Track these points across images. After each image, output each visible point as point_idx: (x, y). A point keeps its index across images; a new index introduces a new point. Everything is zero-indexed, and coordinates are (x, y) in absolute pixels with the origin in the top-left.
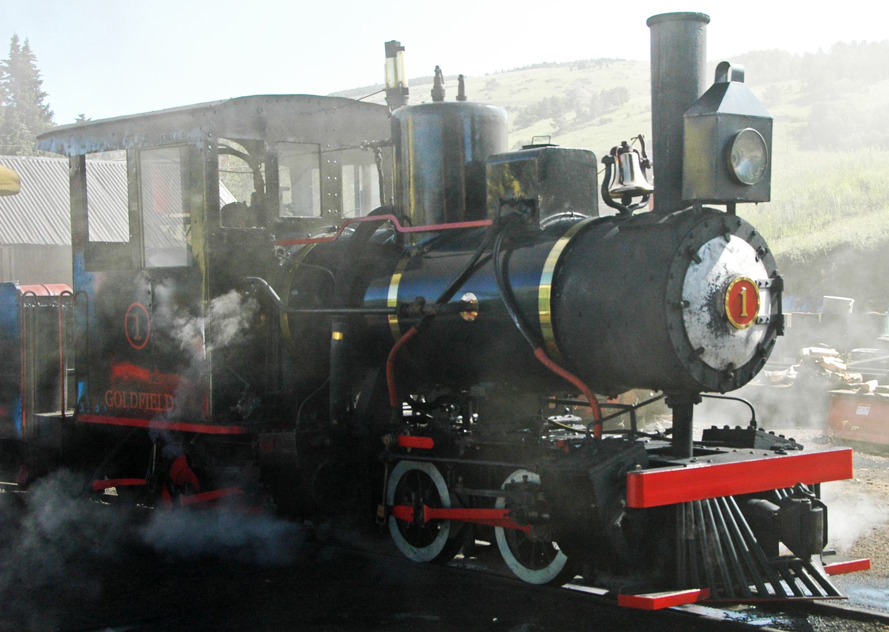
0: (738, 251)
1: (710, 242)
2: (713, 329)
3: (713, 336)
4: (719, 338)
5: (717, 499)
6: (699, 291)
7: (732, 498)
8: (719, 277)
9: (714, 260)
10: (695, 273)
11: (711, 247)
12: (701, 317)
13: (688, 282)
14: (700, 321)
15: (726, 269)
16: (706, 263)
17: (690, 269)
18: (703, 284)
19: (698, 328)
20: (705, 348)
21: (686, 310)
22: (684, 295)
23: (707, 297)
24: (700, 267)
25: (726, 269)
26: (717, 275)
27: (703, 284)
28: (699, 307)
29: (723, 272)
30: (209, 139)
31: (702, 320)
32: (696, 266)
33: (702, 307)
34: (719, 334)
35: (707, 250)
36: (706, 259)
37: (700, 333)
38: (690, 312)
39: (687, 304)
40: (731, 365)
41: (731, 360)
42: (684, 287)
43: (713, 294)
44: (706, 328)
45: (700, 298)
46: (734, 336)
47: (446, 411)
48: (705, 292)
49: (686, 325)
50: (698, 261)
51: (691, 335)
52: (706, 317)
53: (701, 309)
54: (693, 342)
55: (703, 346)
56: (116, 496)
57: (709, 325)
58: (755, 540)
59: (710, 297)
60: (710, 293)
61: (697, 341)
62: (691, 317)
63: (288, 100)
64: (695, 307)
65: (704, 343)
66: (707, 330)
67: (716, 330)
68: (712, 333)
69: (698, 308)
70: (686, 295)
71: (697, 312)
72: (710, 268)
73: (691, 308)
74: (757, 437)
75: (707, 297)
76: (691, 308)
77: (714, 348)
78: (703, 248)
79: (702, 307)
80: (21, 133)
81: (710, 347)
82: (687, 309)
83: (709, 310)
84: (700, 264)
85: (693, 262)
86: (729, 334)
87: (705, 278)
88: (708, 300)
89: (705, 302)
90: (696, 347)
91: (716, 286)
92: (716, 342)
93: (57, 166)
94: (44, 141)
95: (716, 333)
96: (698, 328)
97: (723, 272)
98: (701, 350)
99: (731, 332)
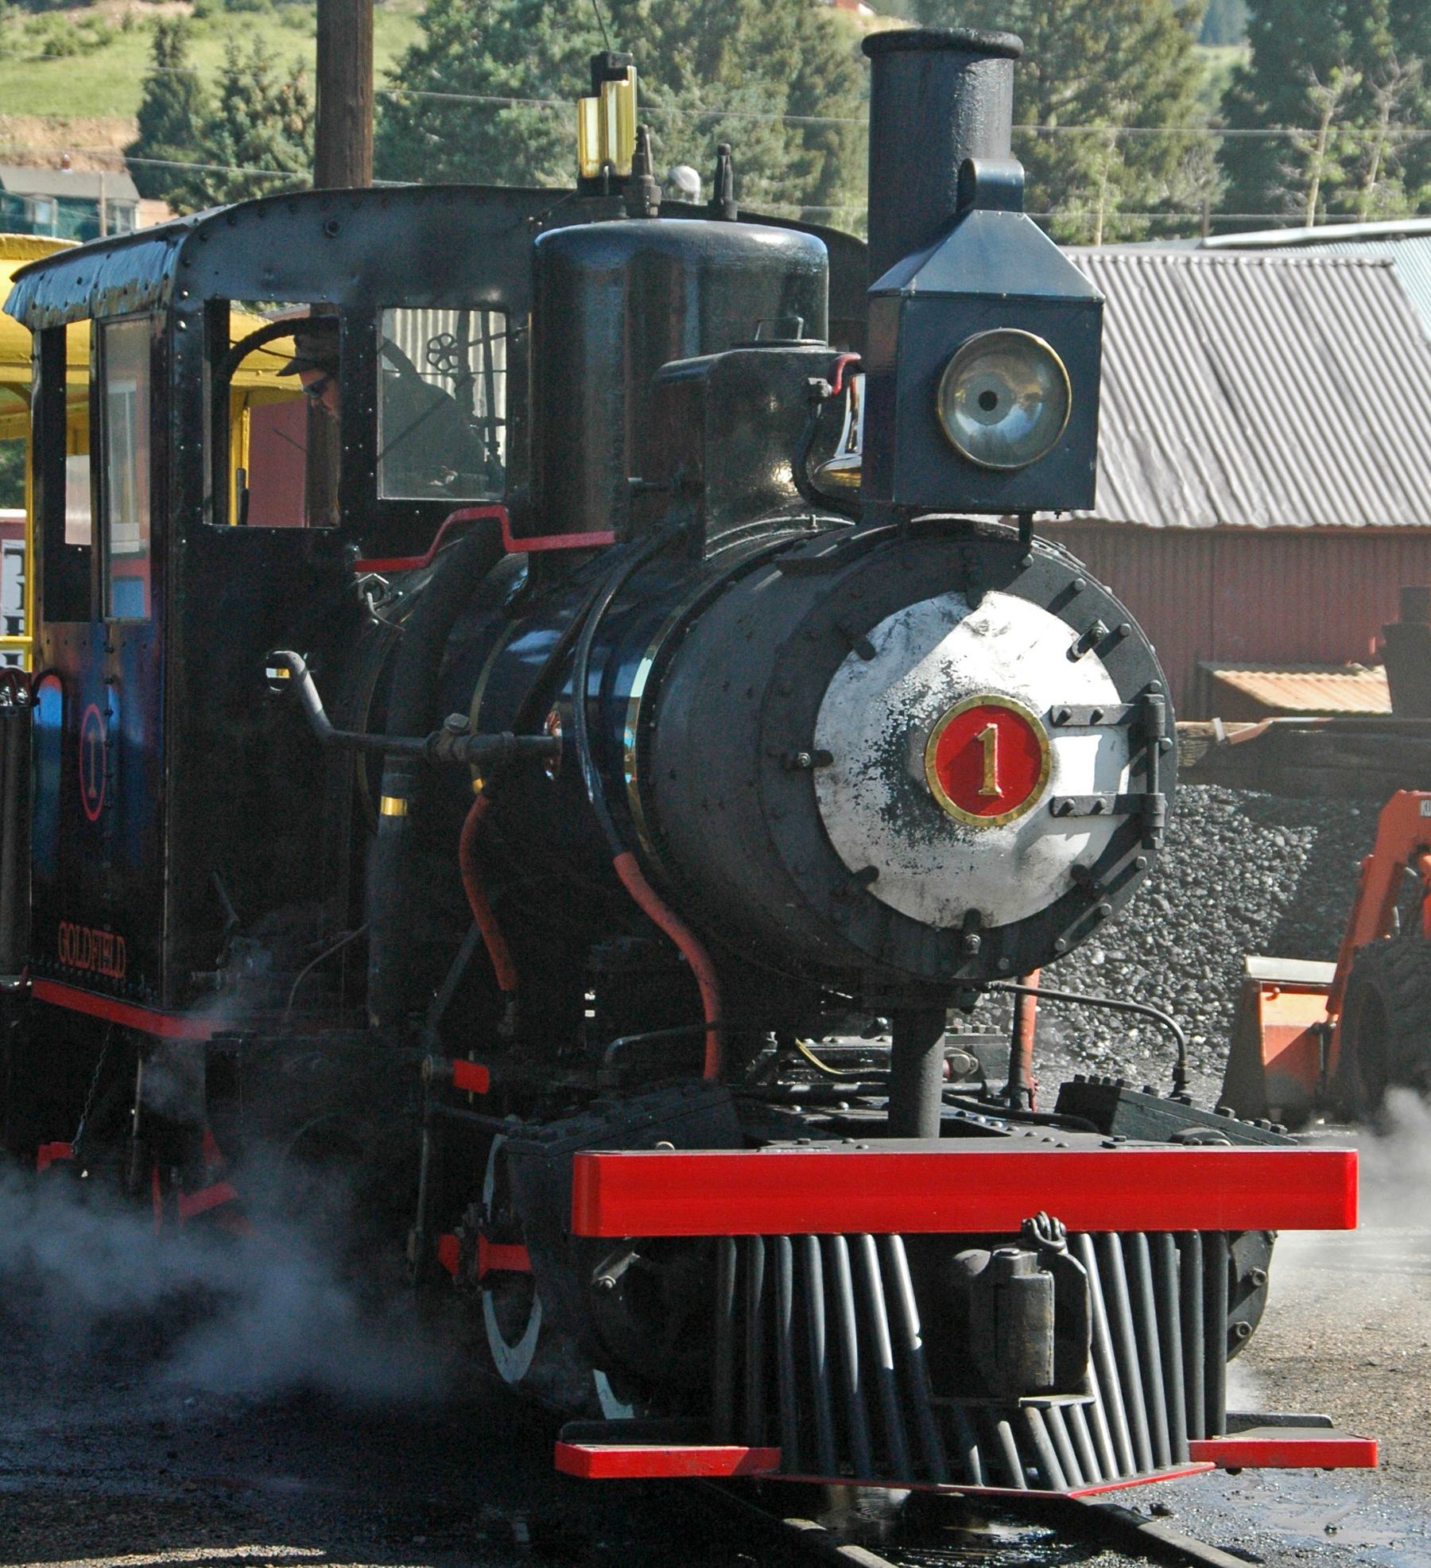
0: (1002, 632)
1: (913, 608)
2: (900, 823)
3: (902, 840)
4: (922, 847)
5: (821, 1237)
6: (861, 729)
7: (898, 1242)
8: (922, 695)
9: (917, 649)
10: (855, 684)
11: (911, 620)
12: (863, 792)
13: (833, 704)
14: (863, 802)
15: (948, 675)
16: (890, 661)
17: (841, 675)
18: (875, 709)
19: (856, 819)
20: (883, 869)
21: (821, 774)
22: (817, 736)
23: (881, 742)
24: (874, 671)
25: (948, 675)
26: (919, 687)
27: (875, 709)
28: (857, 767)
29: (937, 683)
30: (182, 305)
31: (867, 798)
32: (861, 667)
33: (866, 767)
34: (918, 835)
35: (899, 628)
36: (891, 650)
37: (864, 830)
38: (834, 779)
39: (824, 758)
40: (973, 918)
41: (973, 904)
42: (821, 717)
43: (899, 738)
44: (878, 818)
45: (864, 745)
46: (972, 843)
47: (30, 987)
48: (876, 730)
49: (823, 810)
50: (868, 653)
51: (837, 836)
52: (879, 793)
53: (864, 773)
54: (844, 854)
55: (876, 863)
56: (839, 1545)
57: (889, 812)
58: (918, 1343)
59: (890, 743)
60: (892, 735)
61: (858, 851)
62: (835, 793)
63: (262, 215)
64: (848, 766)
65: (877, 857)
66: (881, 825)
67: (912, 824)
68: (898, 832)
69: (856, 770)
70: (824, 735)
71: (854, 780)
72: (901, 671)
73: (838, 770)
74: (1121, 1106)
75: (881, 742)
76: (838, 770)
77: (909, 871)
78: (889, 621)
79: (866, 767)
80: (1072, 140)
81: (895, 867)
82: (826, 771)
83: (887, 775)
84: (872, 662)
85: (853, 655)
86: (952, 835)
87: (880, 696)
88: (885, 751)
89: (875, 755)
90: (855, 867)
91: (911, 717)
92: (912, 855)
93: (1315, 275)
94: (23, 282)
95: (910, 835)
96: (856, 819)
97: (937, 683)
98: (871, 873)
99: (960, 834)
